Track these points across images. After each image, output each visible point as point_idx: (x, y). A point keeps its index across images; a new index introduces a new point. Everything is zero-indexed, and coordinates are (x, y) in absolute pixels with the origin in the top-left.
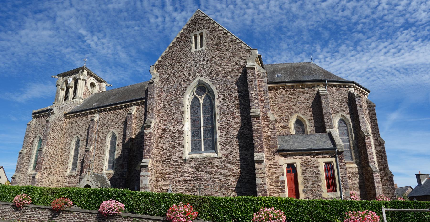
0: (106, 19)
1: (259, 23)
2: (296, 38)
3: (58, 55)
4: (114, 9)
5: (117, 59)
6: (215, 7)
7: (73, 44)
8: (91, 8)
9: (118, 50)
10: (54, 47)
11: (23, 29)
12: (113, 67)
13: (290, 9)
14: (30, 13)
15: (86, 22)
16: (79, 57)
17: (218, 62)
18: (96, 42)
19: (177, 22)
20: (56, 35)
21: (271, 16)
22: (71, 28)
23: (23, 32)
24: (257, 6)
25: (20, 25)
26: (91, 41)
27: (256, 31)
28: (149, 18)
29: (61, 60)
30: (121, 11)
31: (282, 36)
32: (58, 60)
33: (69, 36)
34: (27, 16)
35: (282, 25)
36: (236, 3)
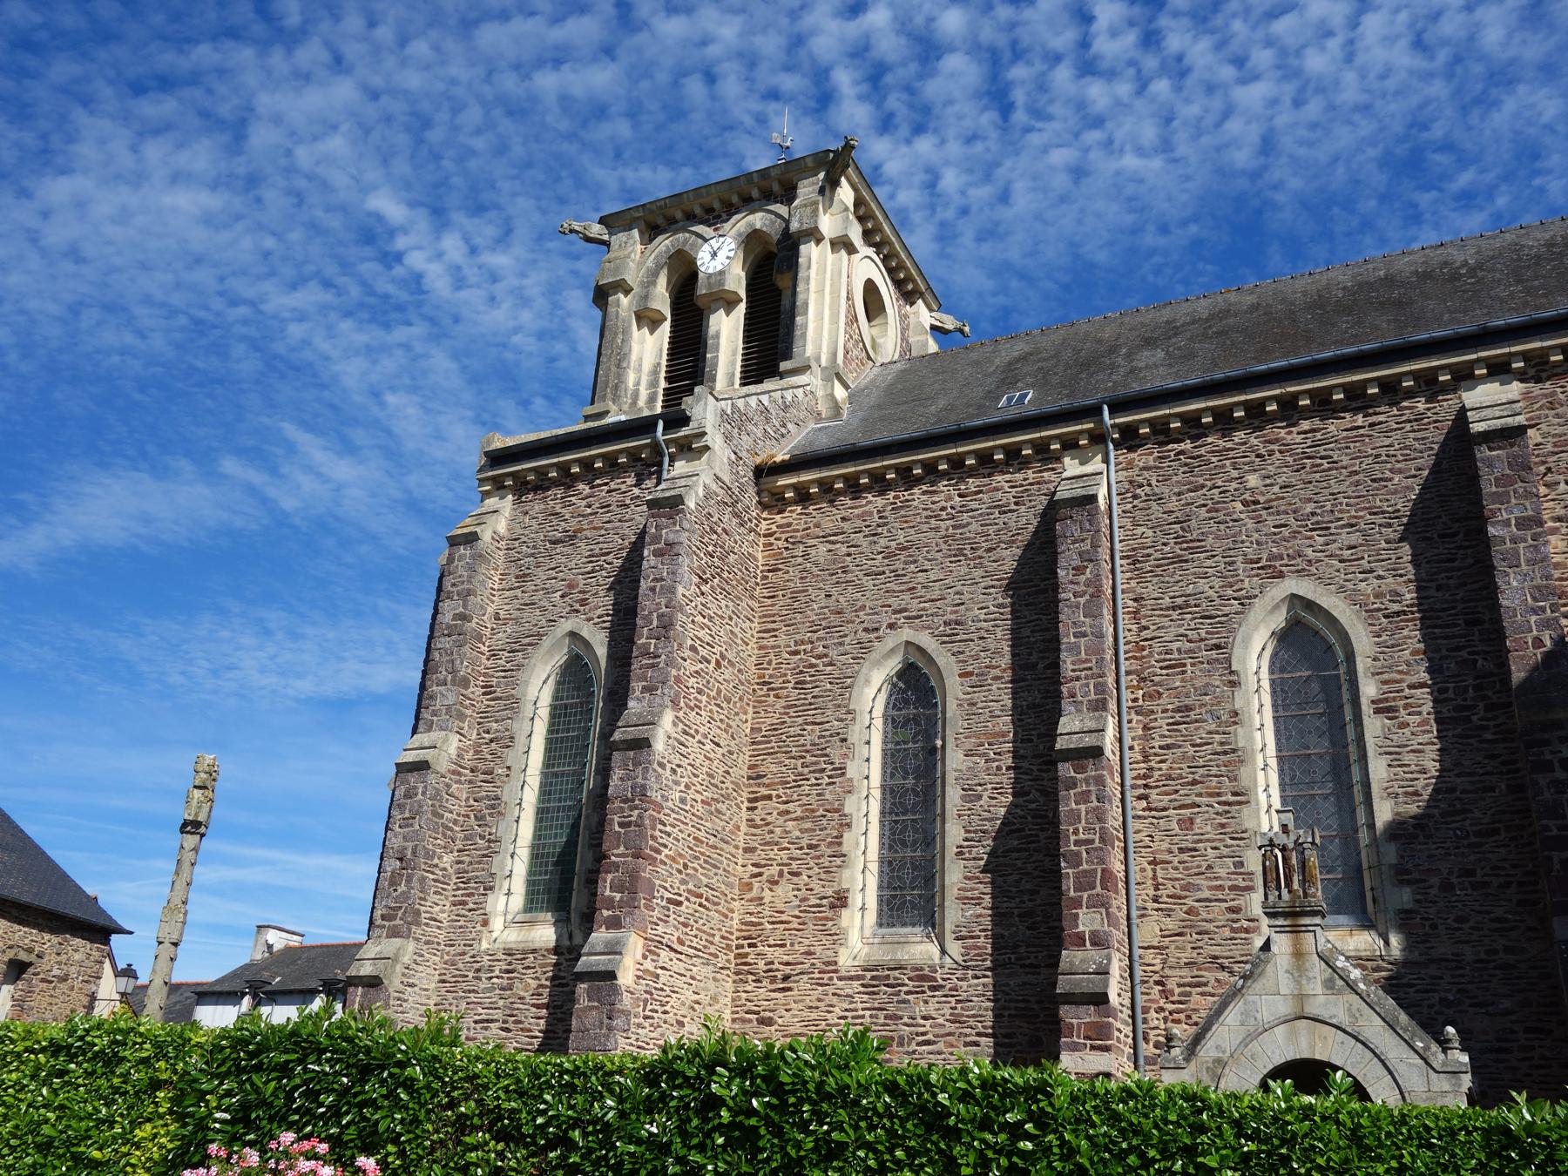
0: (518, 150)
1: (1302, 152)
2: (1502, 201)
3: (245, 322)
4: (565, 100)
5: (563, 363)
6: (1081, 105)
7: (331, 270)
8: (441, 86)
9: (569, 315)
10: (222, 279)
11: (64, 171)
12: (539, 404)
13: (1471, 38)
14: (105, 91)
15: (412, 157)
16: (361, 338)
18: (458, 268)
20: (239, 217)
21: (1364, 98)
22: (325, 186)
23: (57, 190)
24: (1293, 61)
25: (45, 151)
26: (430, 260)
27: (1280, 197)
28: (743, 158)
29: (256, 348)
30: (600, 111)
31: (1425, 199)
32: (239, 350)
33: (314, 227)
34: (87, 102)
35: (1425, 135)
36: (1186, 61)
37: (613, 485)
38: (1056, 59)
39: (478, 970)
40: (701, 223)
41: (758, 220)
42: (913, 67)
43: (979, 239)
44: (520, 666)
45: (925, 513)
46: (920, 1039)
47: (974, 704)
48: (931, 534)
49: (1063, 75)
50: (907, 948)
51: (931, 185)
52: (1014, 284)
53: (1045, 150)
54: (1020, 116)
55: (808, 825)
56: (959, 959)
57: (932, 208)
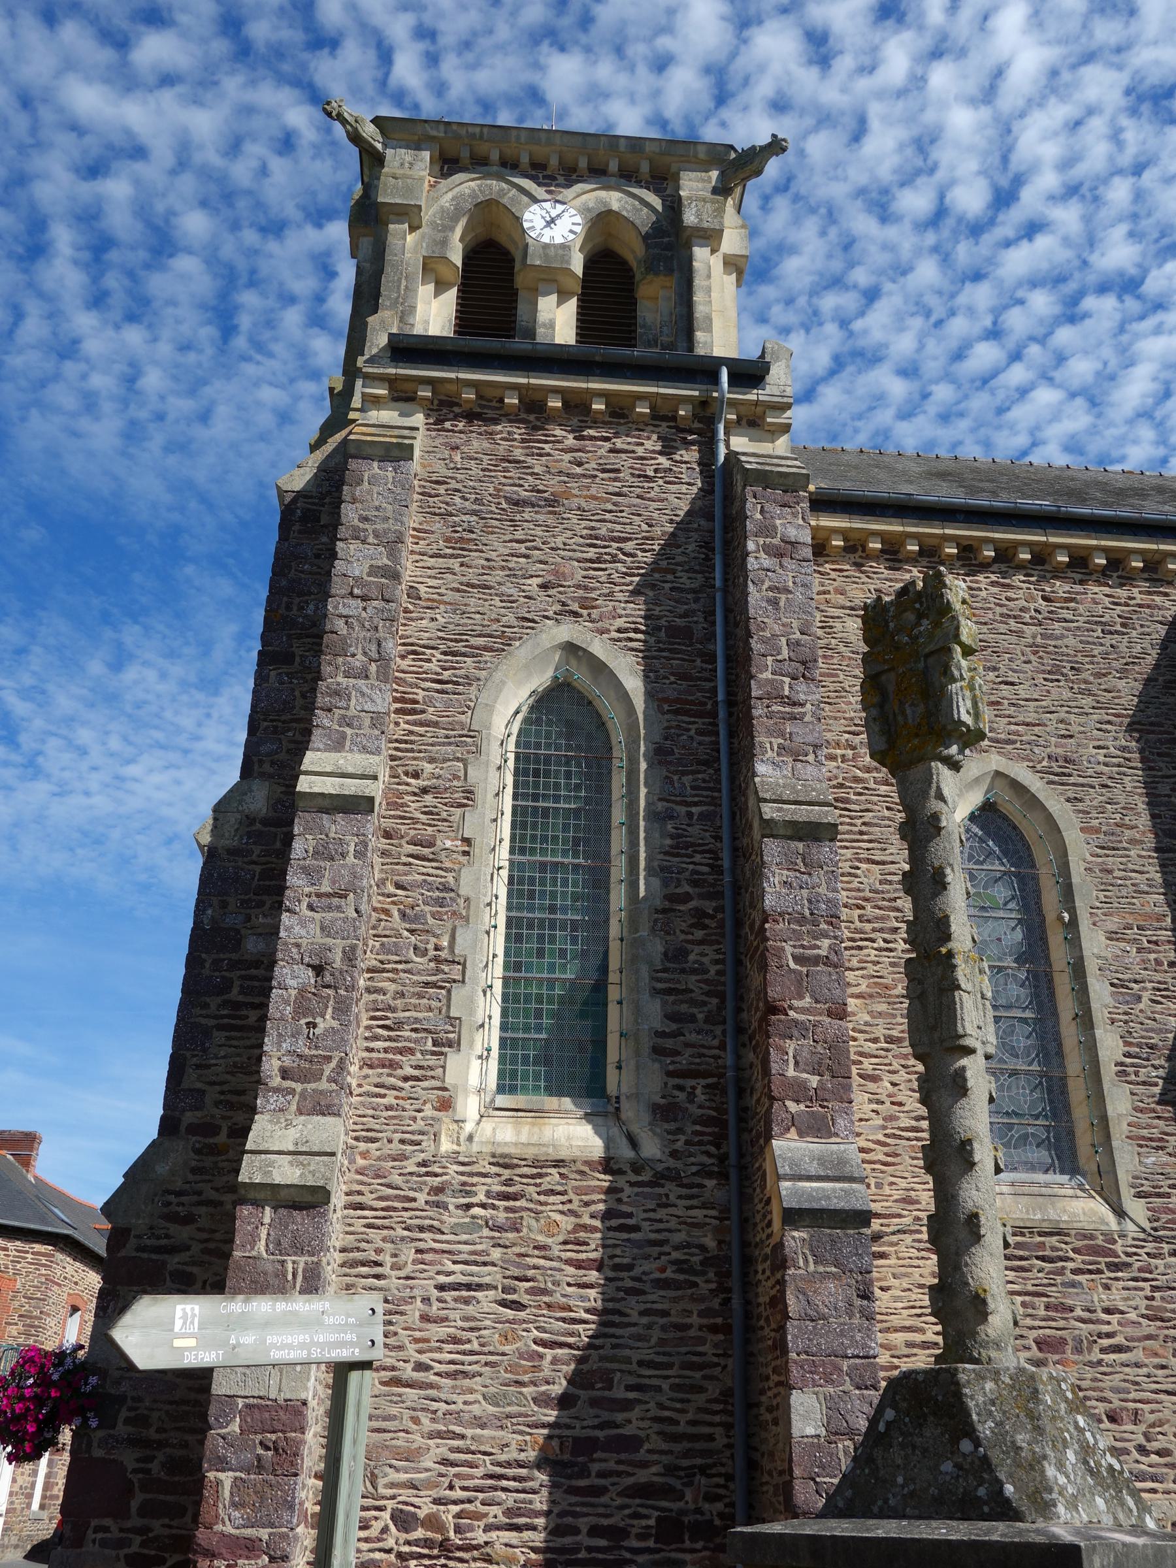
6: (303, 354)
17: (448, 844)
19: (83, 366)
37: (619, 443)
38: (289, 299)
39: (439, 1190)
40: (526, 177)
41: (615, 200)
42: (142, 255)
43: (168, 449)
44: (469, 680)
45: (998, 610)
46: (1106, 1342)
47: (1110, 872)
48: (1014, 639)
49: (292, 318)
50: (1061, 1203)
51: (131, 379)
52: (193, 505)
53: (257, 383)
54: (240, 342)
55: (883, 1007)
56: (1147, 1225)
57: (125, 403)
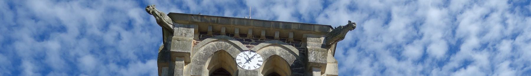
41: (278, 50)
